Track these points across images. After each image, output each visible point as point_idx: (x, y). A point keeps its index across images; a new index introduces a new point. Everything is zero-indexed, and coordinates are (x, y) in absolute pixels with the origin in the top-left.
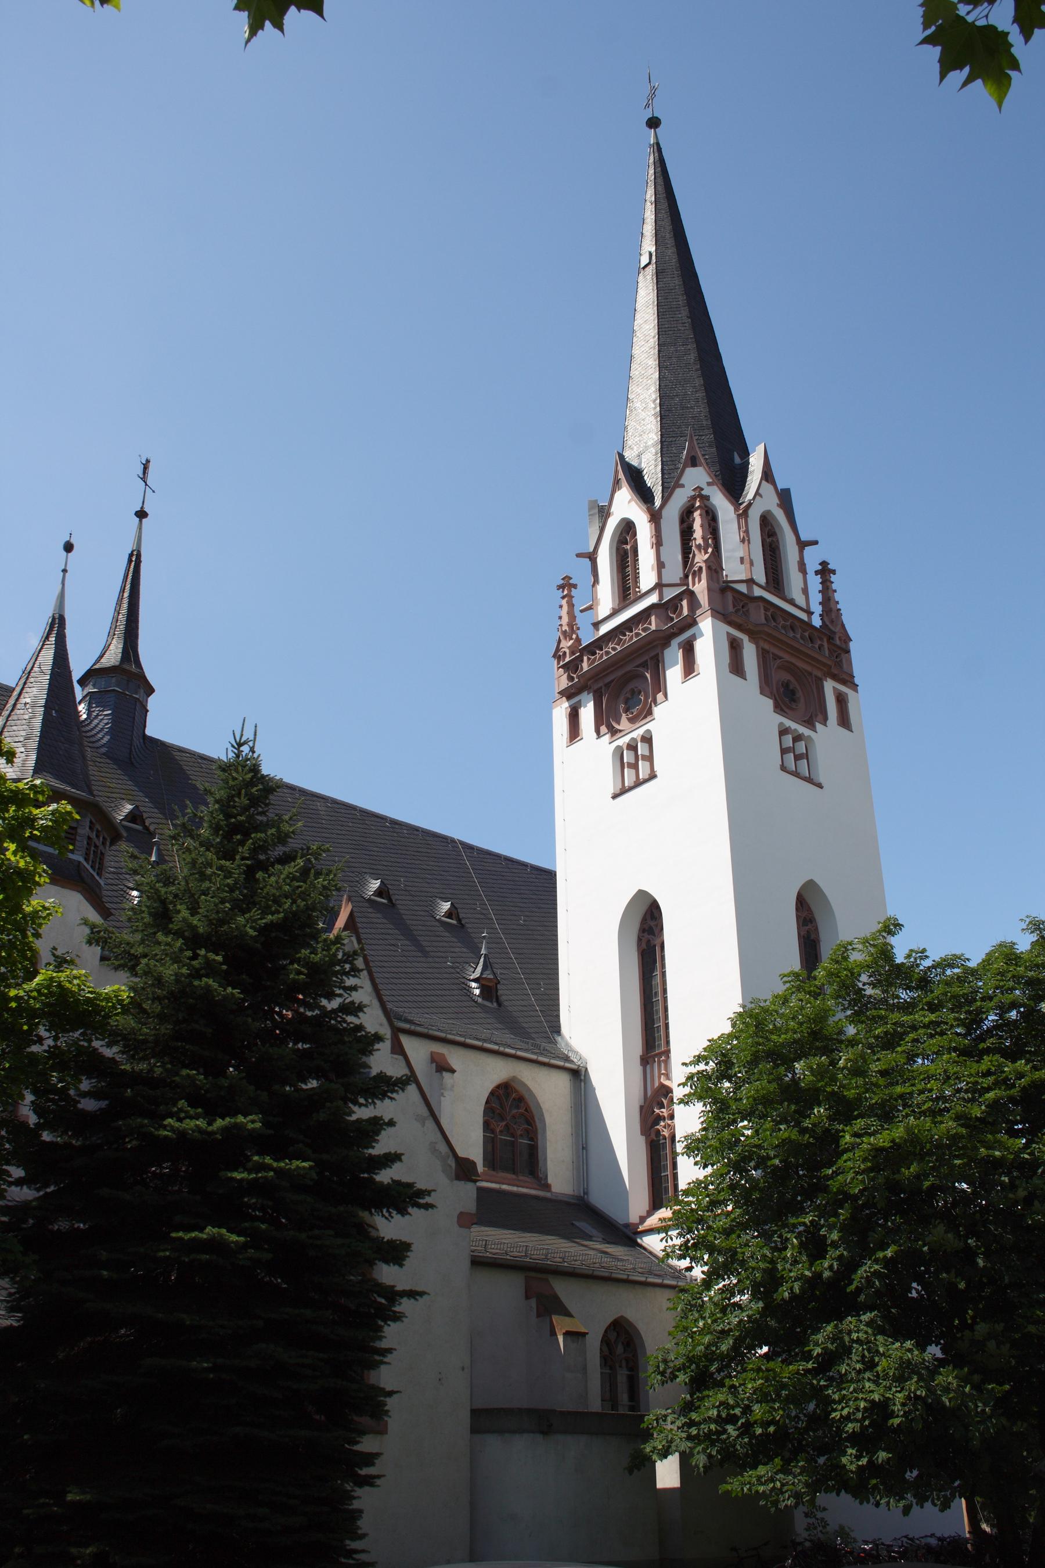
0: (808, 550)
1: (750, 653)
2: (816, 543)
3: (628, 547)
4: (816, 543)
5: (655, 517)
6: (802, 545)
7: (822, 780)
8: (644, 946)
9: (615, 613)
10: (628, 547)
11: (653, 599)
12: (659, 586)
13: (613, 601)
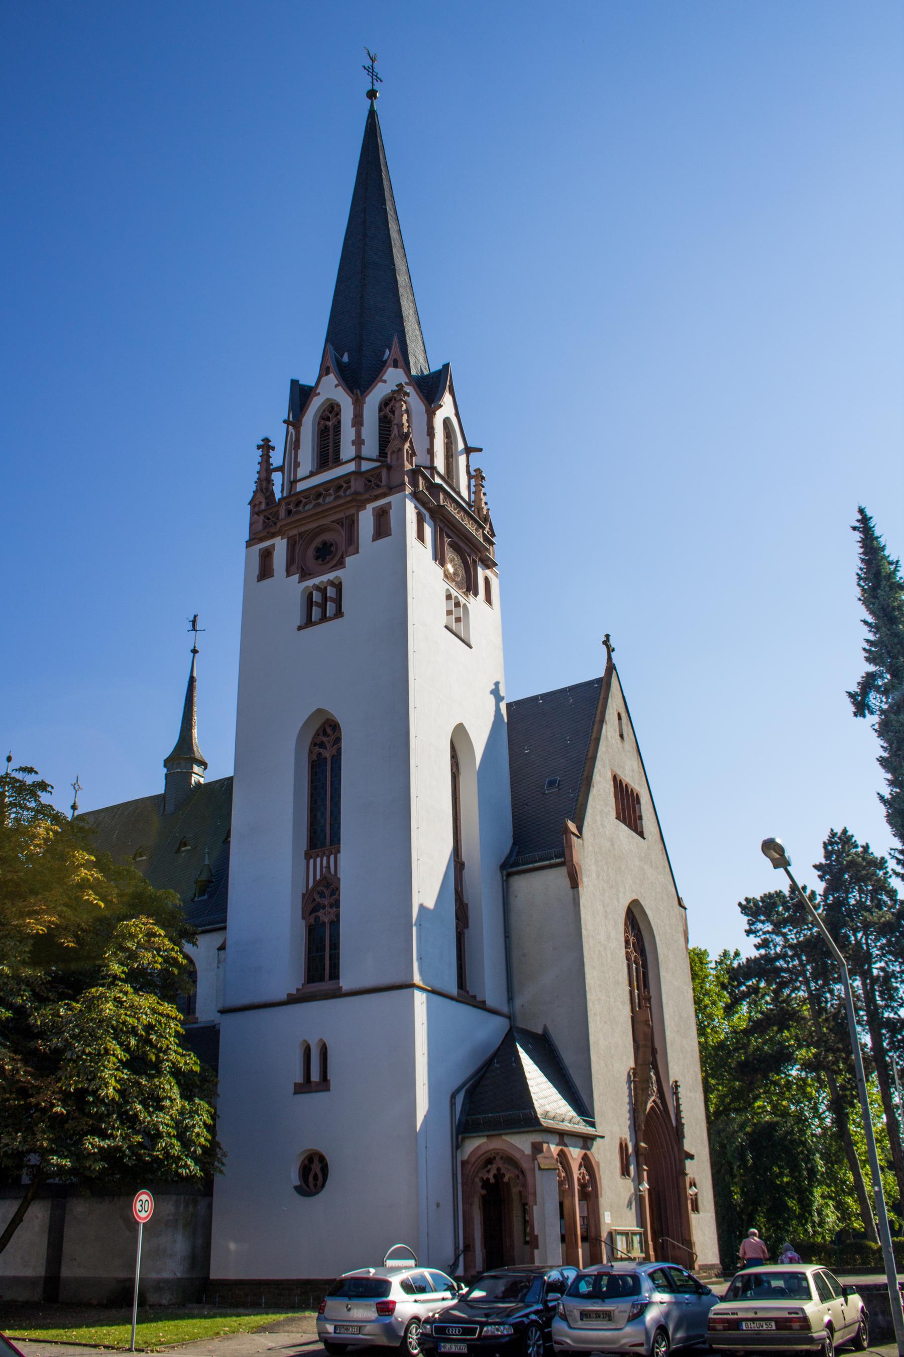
0: (472, 455)
1: (428, 531)
2: (480, 450)
3: (330, 424)
4: (480, 450)
5: (358, 404)
6: (468, 450)
7: (472, 644)
8: (315, 757)
9: (312, 474)
10: (330, 424)
11: (351, 467)
12: (358, 458)
13: (313, 466)
